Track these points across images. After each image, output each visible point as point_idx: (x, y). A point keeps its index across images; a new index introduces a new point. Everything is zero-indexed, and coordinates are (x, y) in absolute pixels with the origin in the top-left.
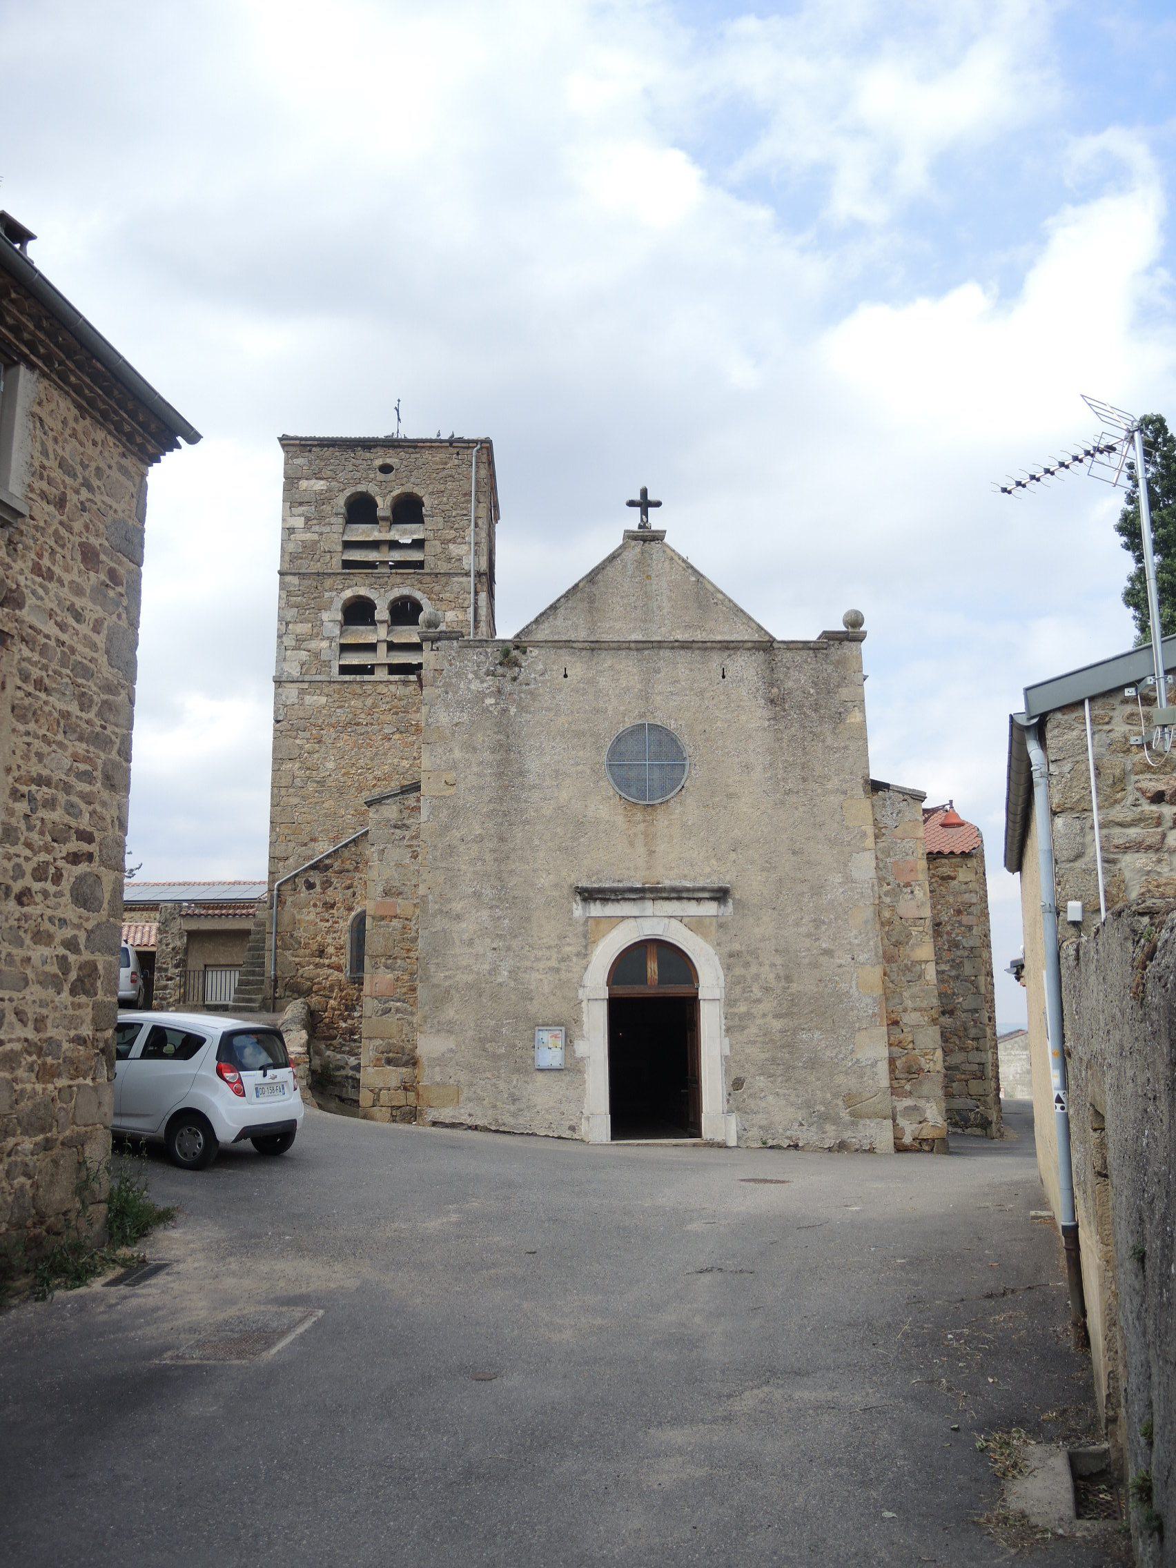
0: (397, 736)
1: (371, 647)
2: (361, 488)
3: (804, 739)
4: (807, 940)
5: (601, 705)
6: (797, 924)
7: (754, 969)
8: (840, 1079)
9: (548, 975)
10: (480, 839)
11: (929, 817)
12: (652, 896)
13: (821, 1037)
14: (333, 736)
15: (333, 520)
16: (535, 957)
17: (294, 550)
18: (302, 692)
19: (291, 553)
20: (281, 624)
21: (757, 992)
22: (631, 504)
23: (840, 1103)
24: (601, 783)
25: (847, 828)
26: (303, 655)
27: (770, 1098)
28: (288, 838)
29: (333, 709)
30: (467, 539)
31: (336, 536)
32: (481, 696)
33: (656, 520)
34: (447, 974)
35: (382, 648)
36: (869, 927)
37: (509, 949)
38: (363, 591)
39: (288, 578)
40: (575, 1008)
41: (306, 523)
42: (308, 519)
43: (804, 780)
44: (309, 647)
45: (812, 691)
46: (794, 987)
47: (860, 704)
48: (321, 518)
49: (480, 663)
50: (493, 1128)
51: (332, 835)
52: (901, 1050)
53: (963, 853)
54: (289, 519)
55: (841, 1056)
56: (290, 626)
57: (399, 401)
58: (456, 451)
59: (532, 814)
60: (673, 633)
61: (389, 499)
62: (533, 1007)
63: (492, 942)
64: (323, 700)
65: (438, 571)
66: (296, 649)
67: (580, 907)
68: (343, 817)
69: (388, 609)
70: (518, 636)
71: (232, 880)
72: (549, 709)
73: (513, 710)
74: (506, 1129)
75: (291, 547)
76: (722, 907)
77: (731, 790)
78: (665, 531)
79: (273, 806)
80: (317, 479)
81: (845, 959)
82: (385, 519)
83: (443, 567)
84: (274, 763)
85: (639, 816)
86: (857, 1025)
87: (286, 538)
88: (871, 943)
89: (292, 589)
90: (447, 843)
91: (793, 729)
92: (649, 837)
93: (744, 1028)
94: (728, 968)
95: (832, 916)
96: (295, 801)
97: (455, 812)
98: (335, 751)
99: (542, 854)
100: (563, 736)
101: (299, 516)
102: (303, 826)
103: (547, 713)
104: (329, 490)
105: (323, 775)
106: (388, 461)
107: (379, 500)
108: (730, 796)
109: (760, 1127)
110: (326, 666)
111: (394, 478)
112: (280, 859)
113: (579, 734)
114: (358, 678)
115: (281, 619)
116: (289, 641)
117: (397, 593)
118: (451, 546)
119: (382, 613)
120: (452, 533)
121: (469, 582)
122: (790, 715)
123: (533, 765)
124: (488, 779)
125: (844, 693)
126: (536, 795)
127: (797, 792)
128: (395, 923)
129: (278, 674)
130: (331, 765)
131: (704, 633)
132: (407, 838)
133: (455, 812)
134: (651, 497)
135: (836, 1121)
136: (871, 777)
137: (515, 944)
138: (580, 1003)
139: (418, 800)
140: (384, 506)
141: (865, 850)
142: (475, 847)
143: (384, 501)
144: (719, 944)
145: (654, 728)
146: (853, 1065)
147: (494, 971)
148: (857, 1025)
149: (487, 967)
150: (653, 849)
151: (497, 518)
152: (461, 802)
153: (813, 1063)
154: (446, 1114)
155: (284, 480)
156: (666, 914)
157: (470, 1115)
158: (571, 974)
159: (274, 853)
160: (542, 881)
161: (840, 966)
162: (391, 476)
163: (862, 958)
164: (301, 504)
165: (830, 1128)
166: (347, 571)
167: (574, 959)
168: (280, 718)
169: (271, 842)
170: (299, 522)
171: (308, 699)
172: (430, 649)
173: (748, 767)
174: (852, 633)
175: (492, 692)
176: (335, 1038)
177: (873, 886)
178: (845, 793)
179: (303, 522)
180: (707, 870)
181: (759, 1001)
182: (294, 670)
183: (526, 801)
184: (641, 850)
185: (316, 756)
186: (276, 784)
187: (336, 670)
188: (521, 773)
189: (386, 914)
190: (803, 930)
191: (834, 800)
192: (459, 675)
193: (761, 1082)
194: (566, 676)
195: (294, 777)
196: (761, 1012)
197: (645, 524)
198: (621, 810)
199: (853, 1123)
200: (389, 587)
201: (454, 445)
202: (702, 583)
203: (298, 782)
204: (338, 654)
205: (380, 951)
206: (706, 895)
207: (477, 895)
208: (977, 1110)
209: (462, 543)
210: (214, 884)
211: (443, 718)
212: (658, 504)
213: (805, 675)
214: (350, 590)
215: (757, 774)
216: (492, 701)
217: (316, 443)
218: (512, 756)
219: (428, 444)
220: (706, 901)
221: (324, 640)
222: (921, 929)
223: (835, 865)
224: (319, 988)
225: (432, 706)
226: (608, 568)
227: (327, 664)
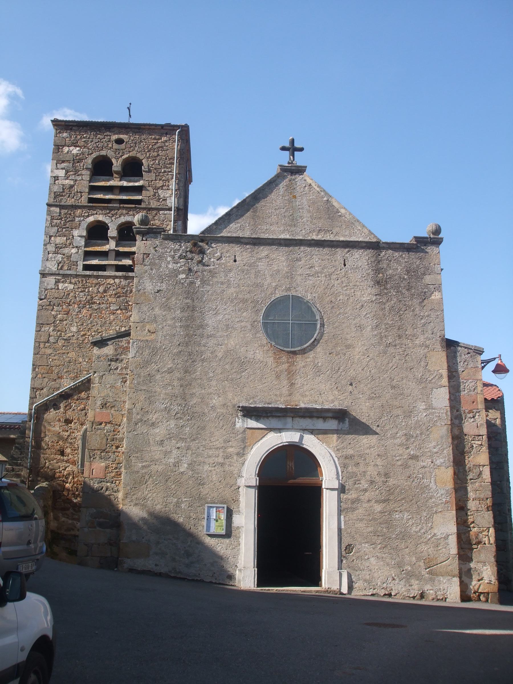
0: (119, 312)
1: (104, 255)
2: (103, 153)
3: (400, 310)
4: (401, 448)
5: (259, 280)
6: (394, 437)
7: (362, 468)
8: (423, 548)
9: (216, 468)
10: (170, 371)
11: (485, 366)
12: (292, 415)
13: (410, 517)
14: (77, 310)
15: (84, 172)
16: (207, 455)
17: (58, 191)
18: (57, 282)
19: (55, 192)
20: (47, 237)
21: (364, 484)
22: (283, 149)
23: (422, 564)
24: (258, 335)
25: (429, 371)
26: (59, 257)
27: (372, 560)
28: (44, 376)
29: (77, 293)
30: (170, 187)
31: (85, 182)
32: (175, 273)
33: (300, 159)
34: (144, 464)
35: (112, 255)
36: (444, 441)
37: (188, 448)
38: (101, 218)
39: (52, 209)
40: (235, 492)
41: (66, 174)
42: (67, 172)
43: (400, 337)
44: (64, 252)
45: (406, 277)
46: (391, 482)
47: (438, 288)
48: (76, 172)
49: (175, 250)
50: (173, 575)
51: (72, 375)
52: (465, 528)
53: (493, 399)
54: (56, 171)
55: (422, 531)
56: (52, 238)
57: (130, 104)
58: (165, 131)
59: (209, 355)
60: (311, 235)
61: (120, 160)
62: (205, 490)
63: (177, 443)
64: (71, 286)
65: (150, 206)
66: (55, 253)
67: (240, 420)
68: (80, 363)
69: (117, 229)
70: (203, 233)
71: (16, 412)
72: (222, 283)
73: (198, 283)
74: (182, 576)
75: (56, 189)
76: (341, 423)
77: (349, 342)
78: (306, 167)
79: (35, 354)
80: (75, 146)
81: (427, 462)
82: (117, 173)
83: (154, 204)
84: (37, 326)
85: (284, 359)
86: (435, 509)
87: (53, 183)
88: (445, 452)
89: (55, 215)
90: (148, 373)
91: (393, 302)
92: (291, 374)
93: (354, 509)
94: (345, 466)
95: (418, 432)
96: (49, 351)
97: (155, 352)
98: (77, 320)
99: (214, 383)
100: (232, 302)
101: (62, 169)
102: (54, 368)
103: (222, 286)
104: (83, 153)
105: (68, 335)
106: (122, 136)
107: (114, 161)
108: (348, 347)
109: (365, 580)
110: (74, 265)
111: (124, 147)
112: (38, 389)
113: (244, 301)
114: (95, 273)
115: (46, 234)
116: (51, 248)
117: (123, 219)
118: (160, 191)
119: (112, 232)
120: (161, 183)
121: (171, 214)
122: (390, 292)
123: (211, 321)
124: (178, 329)
125: (428, 279)
126: (212, 342)
127: (395, 346)
128: (108, 427)
129: (43, 269)
130: (74, 329)
131: (331, 236)
132: (119, 368)
133: (155, 352)
134: (297, 145)
135: (420, 577)
136: (446, 337)
137: (193, 445)
138: (239, 488)
139: (129, 343)
140: (117, 165)
141: (441, 386)
142: (167, 376)
143: (117, 161)
144: (338, 450)
145: (297, 299)
146: (432, 537)
147: (177, 464)
148: (435, 509)
149: (172, 460)
150: (293, 381)
151: (190, 181)
152: (159, 345)
153: (404, 536)
154: (140, 564)
155: (53, 147)
156: (301, 428)
157: (156, 565)
158: (232, 467)
159: (34, 385)
160: (214, 401)
161: (424, 467)
162: (123, 146)
163: (438, 462)
164: (63, 162)
165: (415, 583)
166: (91, 204)
167: (235, 457)
168: (43, 297)
169: (32, 378)
170: (61, 173)
171: (61, 286)
172: (141, 240)
173: (360, 327)
174: (433, 238)
175: (184, 270)
176: (68, 509)
177: (447, 412)
178: (427, 347)
179: (64, 173)
180: (331, 398)
181: (366, 490)
182: (52, 267)
183: (205, 346)
184: (285, 382)
185: (65, 323)
186: (38, 340)
187: (80, 267)
188: (202, 326)
189: (102, 421)
190: (398, 441)
191: (422, 351)
192: (160, 257)
193: (366, 547)
194: (235, 261)
195: (49, 336)
196: (367, 499)
197: (292, 162)
198: (271, 354)
199: (431, 579)
200: (118, 216)
201: (164, 128)
202: (330, 202)
203: (52, 339)
204: (82, 257)
205: (97, 446)
206: (330, 415)
207: (167, 410)
208: (501, 572)
209: (168, 189)
210: (4, 414)
211: (149, 286)
212: (301, 150)
213: (401, 266)
214: (93, 216)
215: (368, 331)
216: (184, 276)
217: (75, 124)
218: (196, 314)
219: (148, 127)
220: (330, 420)
221: (74, 248)
222: (480, 443)
223: (420, 396)
224: (59, 476)
225: (141, 278)
226: (266, 190)
227: (76, 264)
